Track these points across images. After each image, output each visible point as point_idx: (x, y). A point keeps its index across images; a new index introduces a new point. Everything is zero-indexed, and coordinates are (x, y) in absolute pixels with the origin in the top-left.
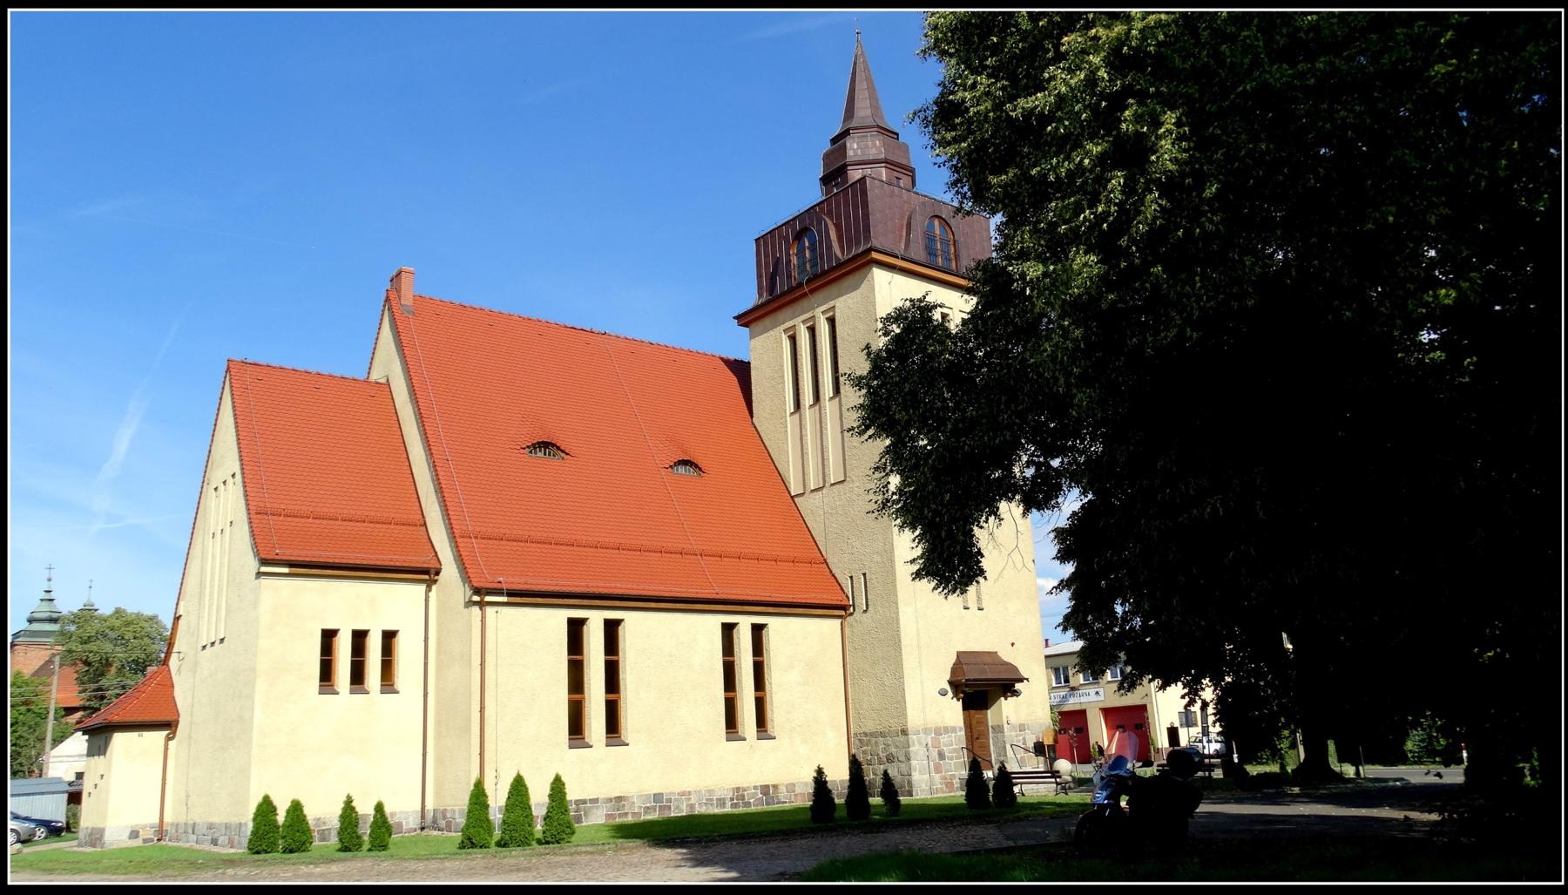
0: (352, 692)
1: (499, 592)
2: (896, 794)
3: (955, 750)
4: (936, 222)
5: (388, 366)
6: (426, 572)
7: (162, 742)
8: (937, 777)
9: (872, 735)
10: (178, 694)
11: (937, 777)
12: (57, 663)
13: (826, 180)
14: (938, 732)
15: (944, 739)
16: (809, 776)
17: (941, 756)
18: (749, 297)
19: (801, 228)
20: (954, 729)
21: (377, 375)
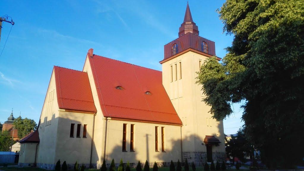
0: (130, 152)
1: (110, 117)
2: (195, 166)
3: (205, 157)
4: (204, 43)
5: (88, 69)
6: (94, 112)
7: (36, 146)
8: (201, 163)
9: (187, 152)
10: (40, 136)
11: (201, 163)
12: (14, 128)
13: (179, 34)
14: (201, 153)
15: (202, 154)
16: (192, 162)
17: (202, 158)
18: (163, 58)
19: (174, 42)
20: (205, 152)
21: (85, 71)
